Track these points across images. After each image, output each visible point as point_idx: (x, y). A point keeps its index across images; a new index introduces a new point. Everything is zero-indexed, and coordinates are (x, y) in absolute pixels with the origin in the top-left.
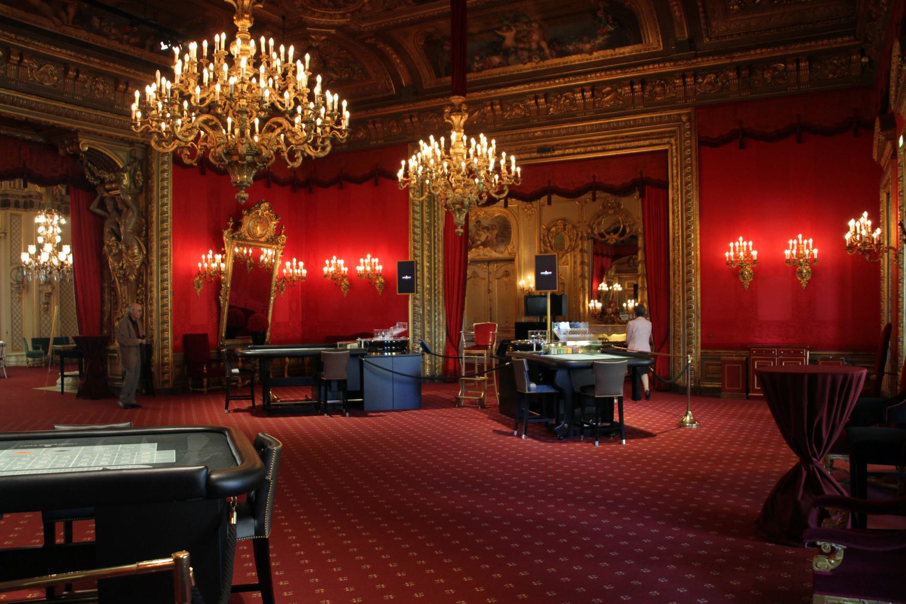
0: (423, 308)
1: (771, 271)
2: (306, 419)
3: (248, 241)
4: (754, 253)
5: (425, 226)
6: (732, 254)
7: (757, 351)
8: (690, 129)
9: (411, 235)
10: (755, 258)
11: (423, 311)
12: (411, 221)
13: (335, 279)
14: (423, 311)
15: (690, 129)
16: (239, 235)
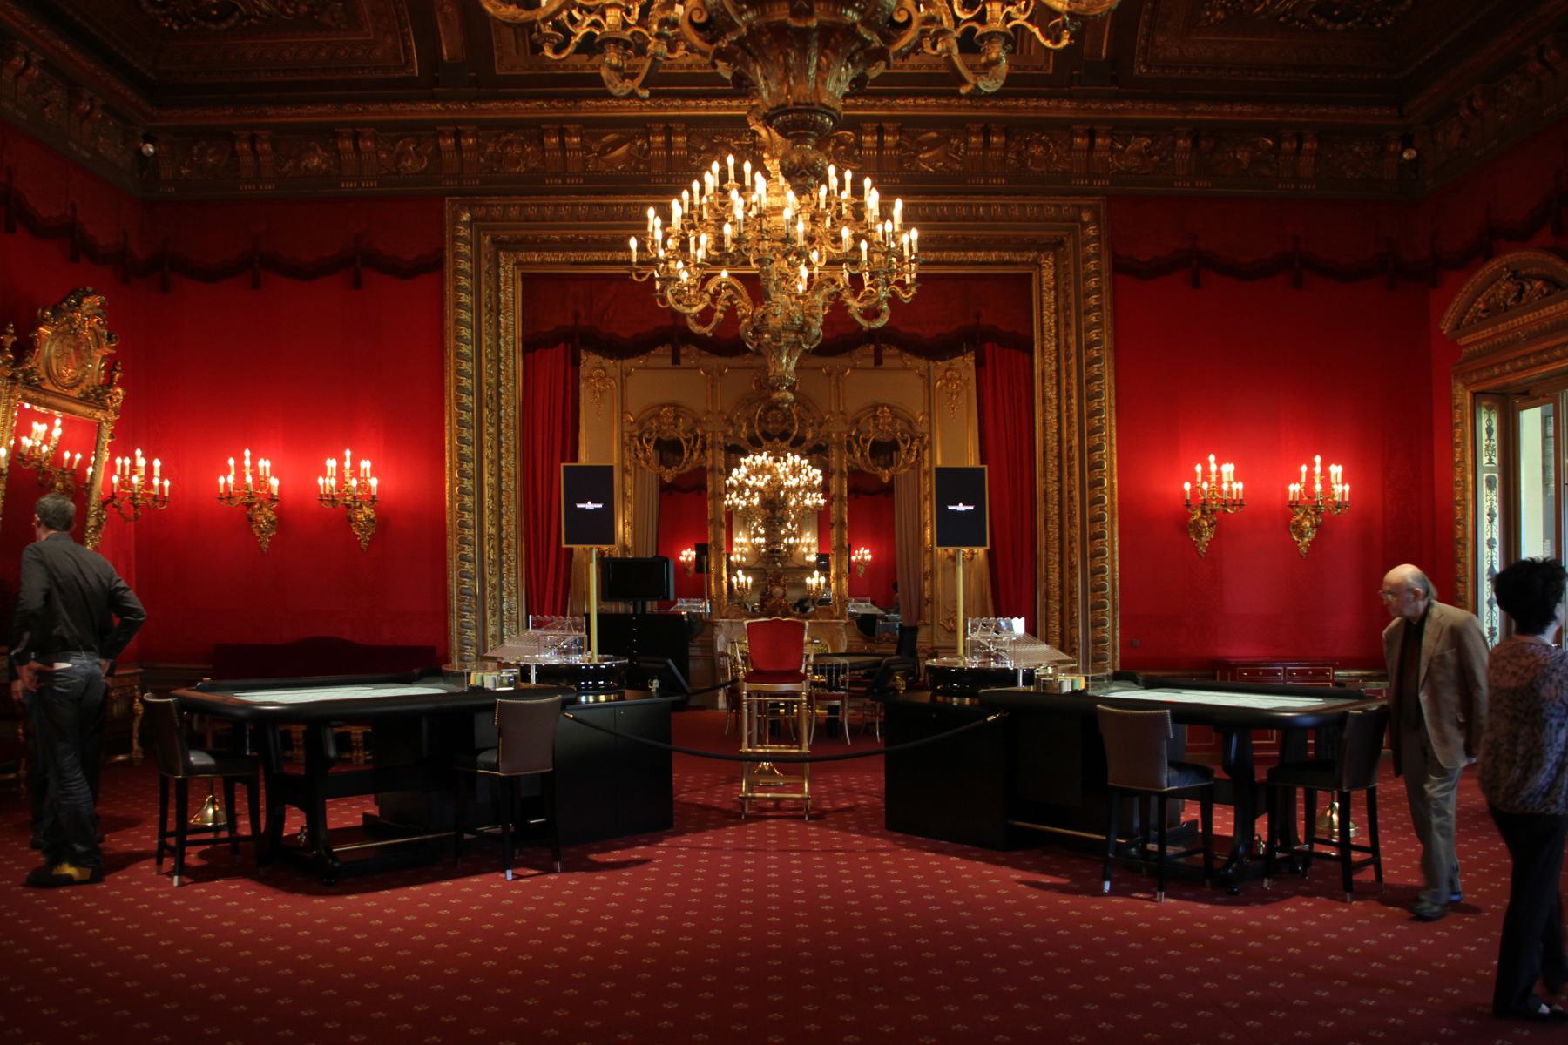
0: (483, 579)
1: (1266, 520)
2: (370, 901)
3: (47, 392)
4: (274, 482)
5: (486, 391)
6: (231, 479)
7: (1250, 673)
8: (1098, 239)
9: (450, 409)
10: (374, 492)
11: (483, 589)
12: (450, 379)
13: (242, 509)
14: (483, 589)
15: (1098, 239)
16: (27, 374)
